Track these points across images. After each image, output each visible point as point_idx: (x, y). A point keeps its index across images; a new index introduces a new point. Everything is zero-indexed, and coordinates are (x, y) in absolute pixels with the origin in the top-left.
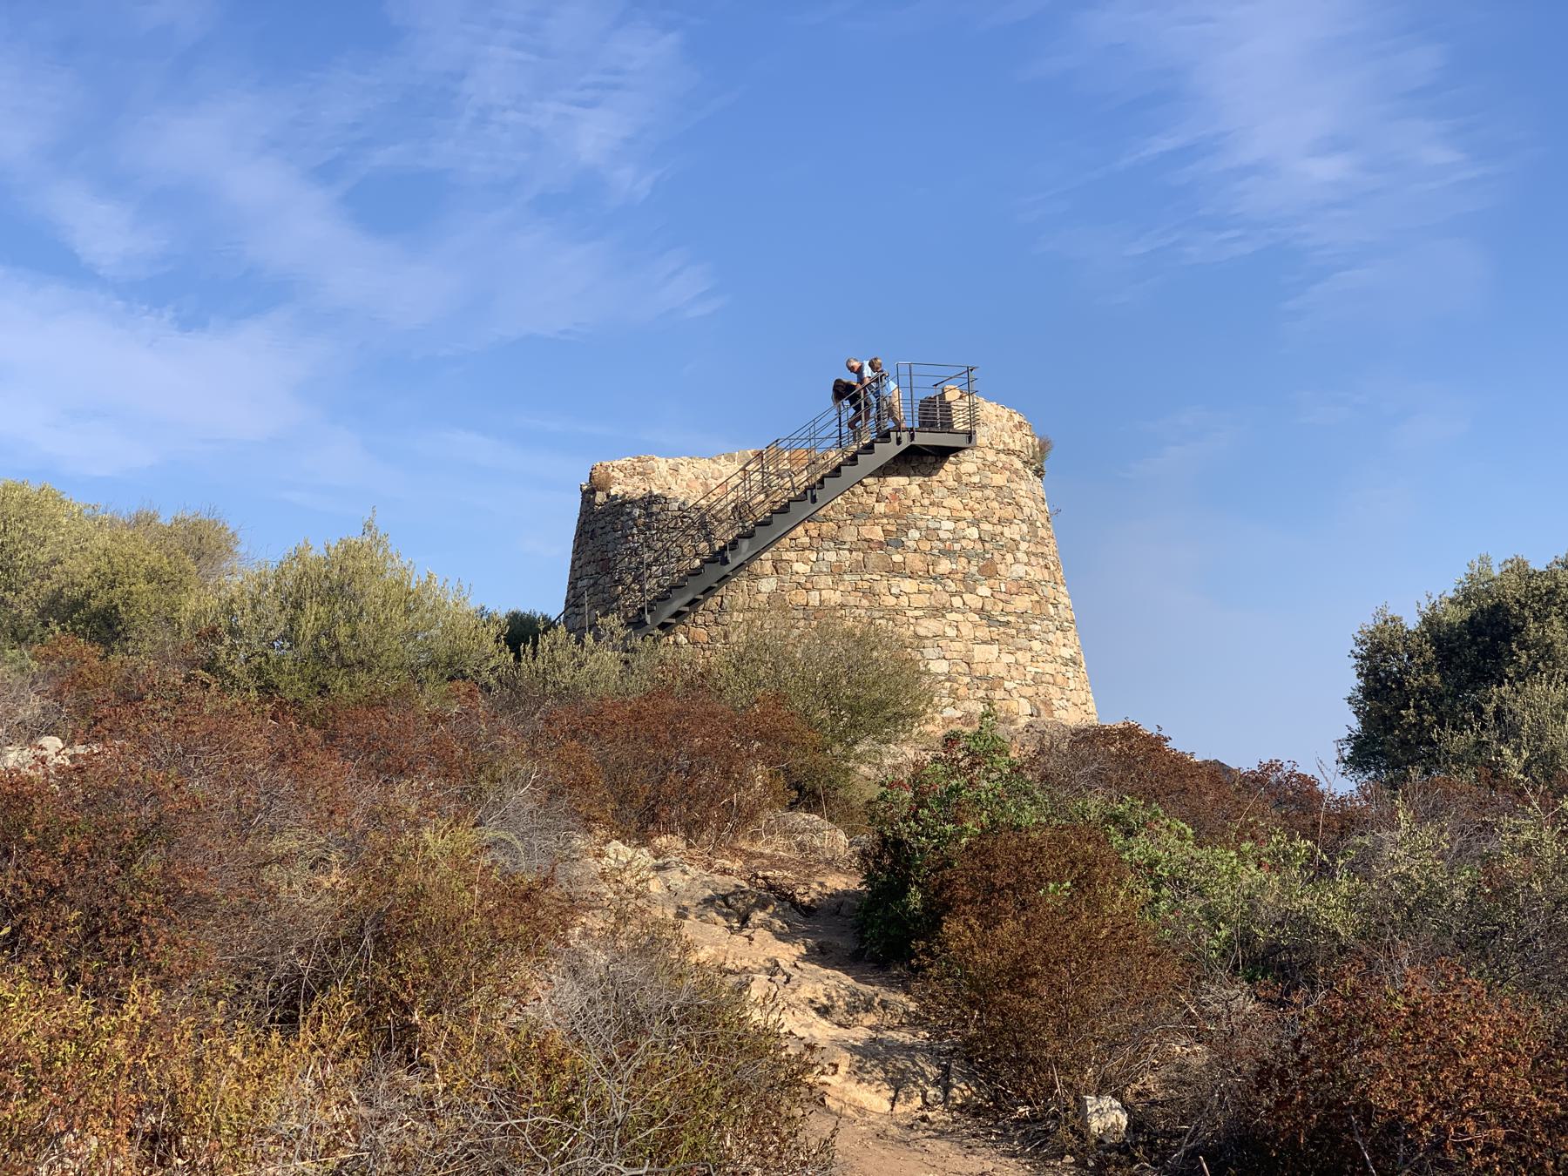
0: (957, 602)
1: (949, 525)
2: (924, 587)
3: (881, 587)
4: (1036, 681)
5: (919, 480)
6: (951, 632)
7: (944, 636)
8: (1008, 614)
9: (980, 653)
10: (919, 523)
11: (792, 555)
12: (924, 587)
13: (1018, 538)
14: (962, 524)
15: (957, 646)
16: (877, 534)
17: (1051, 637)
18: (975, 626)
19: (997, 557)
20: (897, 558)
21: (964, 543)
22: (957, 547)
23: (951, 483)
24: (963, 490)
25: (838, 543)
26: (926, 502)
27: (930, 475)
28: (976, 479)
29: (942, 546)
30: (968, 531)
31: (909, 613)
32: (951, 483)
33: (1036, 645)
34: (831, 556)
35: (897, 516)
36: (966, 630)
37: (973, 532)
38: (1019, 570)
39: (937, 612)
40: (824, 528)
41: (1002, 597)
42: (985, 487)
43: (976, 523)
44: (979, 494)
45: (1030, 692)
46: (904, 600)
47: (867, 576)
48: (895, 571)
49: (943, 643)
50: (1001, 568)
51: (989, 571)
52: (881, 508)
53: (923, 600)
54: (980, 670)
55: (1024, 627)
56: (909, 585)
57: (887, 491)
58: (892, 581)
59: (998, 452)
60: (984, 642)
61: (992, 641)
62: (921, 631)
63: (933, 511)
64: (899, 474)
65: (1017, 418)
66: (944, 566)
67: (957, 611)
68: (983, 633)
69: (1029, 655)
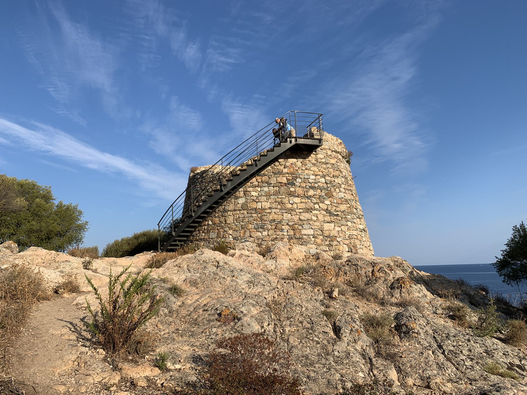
0: (317, 206)
1: (313, 177)
2: (303, 200)
3: (286, 201)
4: (350, 238)
5: (301, 160)
6: (315, 218)
7: (311, 220)
8: (337, 211)
9: (327, 226)
10: (301, 176)
11: (251, 189)
12: (303, 200)
13: (341, 183)
14: (318, 177)
15: (317, 224)
16: (284, 180)
17: (355, 221)
18: (324, 216)
19: (333, 190)
20: (292, 189)
21: (319, 184)
22: (316, 185)
23: (314, 161)
24: (318, 164)
25: (269, 184)
26: (304, 168)
27: (305, 158)
28: (324, 160)
29: (310, 185)
30: (321, 180)
31: (297, 211)
32: (314, 161)
33: (349, 224)
34: (266, 189)
35: (292, 174)
36: (321, 217)
37: (323, 180)
38: (342, 195)
39: (309, 210)
40: (264, 178)
41: (335, 205)
42: (327, 163)
43: (324, 176)
44: (325, 166)
45: (347, 242)
46: (295, 206)
47: (280, 197)
48: (291, 194)
49: (311, 222)
50: (334, 194)
51: (329, 195)
52: (286, 170)
53: (303, 206)
54: (327, 233)
55: (344, 216)
56: (297, 200)
57: (288, 164)
58: (290, 198)
59: (332, 151)
60: (328, 222)
61: (331, 222)
62: (302, 218)
63: (306, 172)
64: (293, 158)
65: (339, 141)
66: (311, 192)
67: (317, 210)
68: (328, 218)
69: (346, 227)
